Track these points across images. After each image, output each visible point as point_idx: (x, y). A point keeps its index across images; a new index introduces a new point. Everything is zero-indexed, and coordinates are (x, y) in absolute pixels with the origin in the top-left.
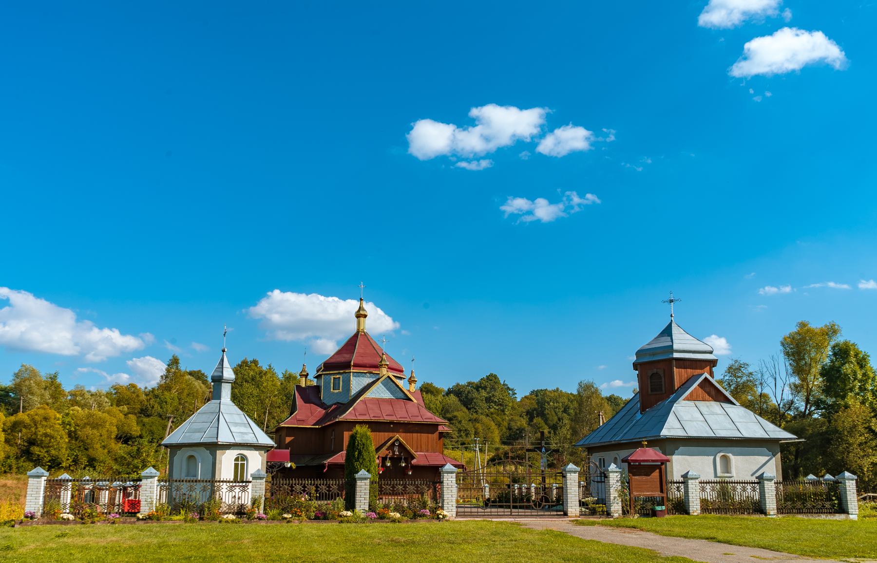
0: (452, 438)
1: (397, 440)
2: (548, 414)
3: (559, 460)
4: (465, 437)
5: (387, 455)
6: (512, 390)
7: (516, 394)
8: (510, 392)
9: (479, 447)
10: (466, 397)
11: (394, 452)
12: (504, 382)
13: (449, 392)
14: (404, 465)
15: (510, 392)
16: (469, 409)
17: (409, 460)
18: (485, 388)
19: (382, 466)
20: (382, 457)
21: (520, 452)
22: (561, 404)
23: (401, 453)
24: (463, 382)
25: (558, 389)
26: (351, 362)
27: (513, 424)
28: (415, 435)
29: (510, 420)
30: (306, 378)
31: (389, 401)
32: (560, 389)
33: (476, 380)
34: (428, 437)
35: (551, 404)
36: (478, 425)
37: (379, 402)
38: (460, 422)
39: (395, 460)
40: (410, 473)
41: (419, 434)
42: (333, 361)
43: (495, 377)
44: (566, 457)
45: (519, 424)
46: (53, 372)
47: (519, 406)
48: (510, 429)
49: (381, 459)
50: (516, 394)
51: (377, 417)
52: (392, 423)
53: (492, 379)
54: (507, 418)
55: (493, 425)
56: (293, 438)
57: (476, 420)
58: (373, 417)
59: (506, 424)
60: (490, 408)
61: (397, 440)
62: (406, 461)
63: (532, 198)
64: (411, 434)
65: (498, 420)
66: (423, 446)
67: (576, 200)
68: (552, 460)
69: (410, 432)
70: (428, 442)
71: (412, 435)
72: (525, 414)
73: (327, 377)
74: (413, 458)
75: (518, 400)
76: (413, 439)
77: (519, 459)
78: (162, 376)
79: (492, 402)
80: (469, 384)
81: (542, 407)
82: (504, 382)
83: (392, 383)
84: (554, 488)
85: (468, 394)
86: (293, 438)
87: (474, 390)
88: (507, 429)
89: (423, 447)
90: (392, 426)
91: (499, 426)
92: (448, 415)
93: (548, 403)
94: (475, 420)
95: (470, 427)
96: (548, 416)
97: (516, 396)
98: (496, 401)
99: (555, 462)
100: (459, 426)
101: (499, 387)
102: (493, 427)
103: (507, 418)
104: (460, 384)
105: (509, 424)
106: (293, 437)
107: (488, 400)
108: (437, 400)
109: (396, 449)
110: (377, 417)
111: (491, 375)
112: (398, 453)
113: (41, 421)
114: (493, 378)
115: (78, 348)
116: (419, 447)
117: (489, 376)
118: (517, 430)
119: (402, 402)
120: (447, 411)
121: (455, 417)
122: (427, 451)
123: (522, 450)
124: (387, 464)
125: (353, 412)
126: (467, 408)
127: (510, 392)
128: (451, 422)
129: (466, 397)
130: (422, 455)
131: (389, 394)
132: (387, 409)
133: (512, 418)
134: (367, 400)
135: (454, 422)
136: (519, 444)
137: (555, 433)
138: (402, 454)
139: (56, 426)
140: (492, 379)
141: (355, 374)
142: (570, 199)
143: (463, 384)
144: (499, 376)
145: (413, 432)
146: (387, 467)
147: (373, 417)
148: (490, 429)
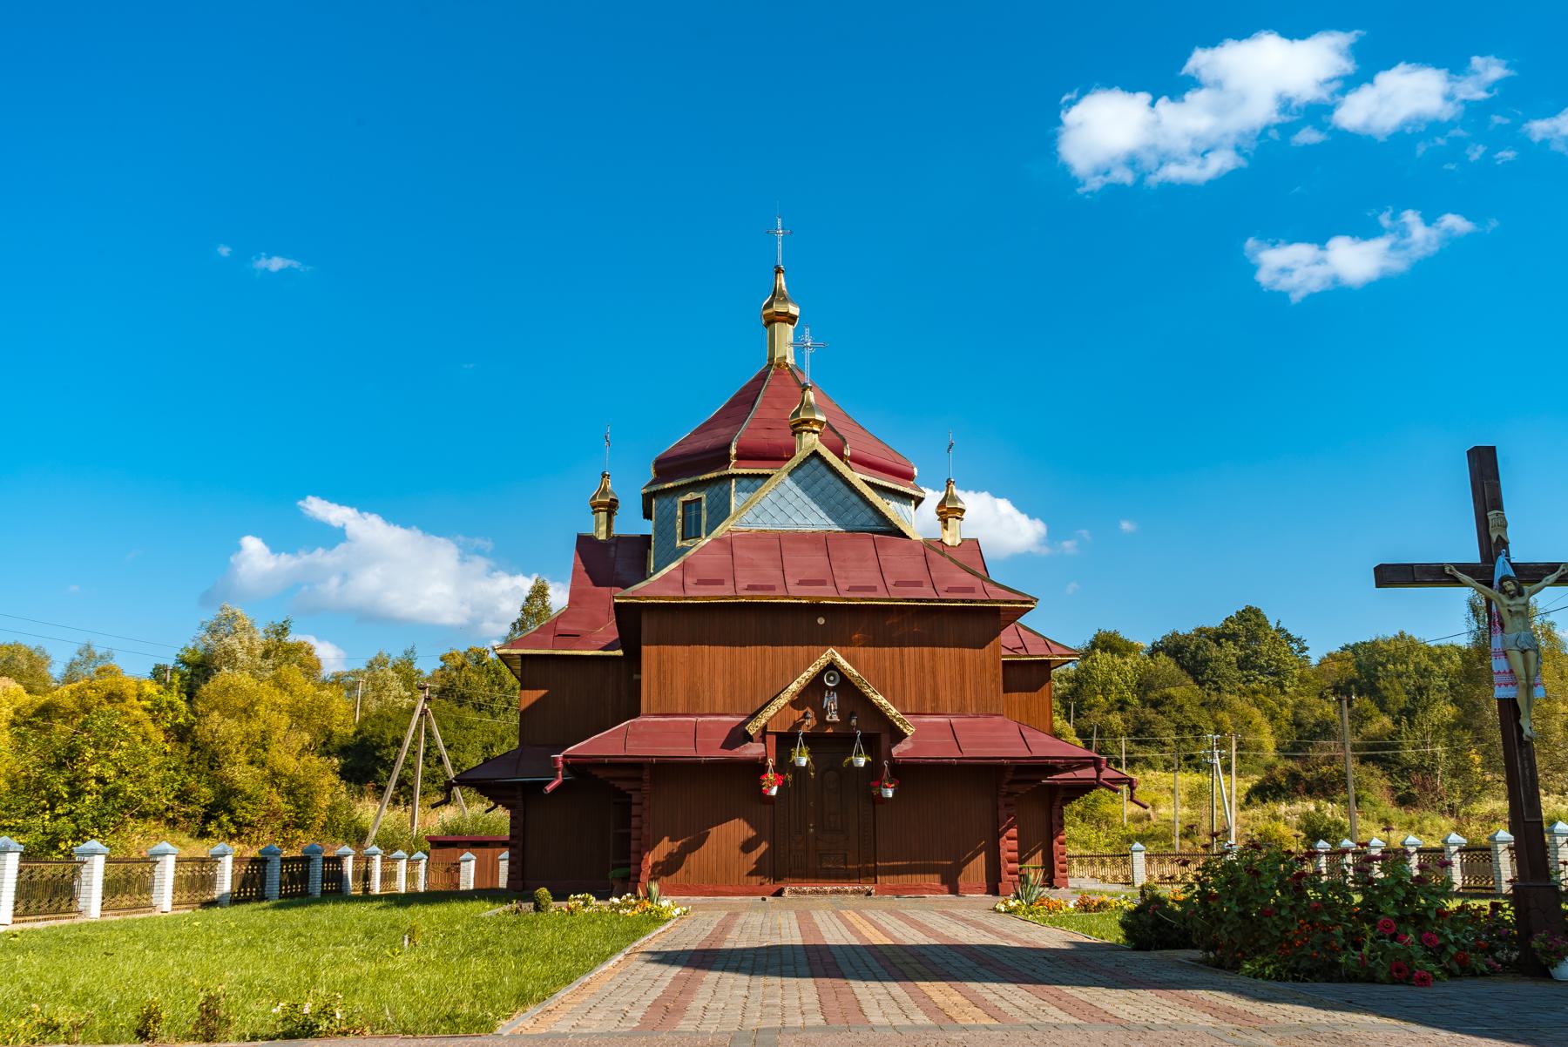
0: (1164, 744)
1: (832, 666)
2: (1386, 688)
3: (1424, 787)
4: (1193, 743)
5: (798, 725)
6: (1298, 641)
7: (1307, 649)
8: (1295, 646)
9: (1220, 755)
10: (1194, 657)
11: (821, 713)
12: (1278, 624)
13: (1155, 650)
14: (862, 761)
15: (1295, 646)
16: (1201, 684)
17: (884, 745)
18: (1233, 637)
19: (777, 769)
20: (777, 734)
21: (1324, 769)
22: (1411, 667)
23: (852, 714)
24: (1186, 629)
25: (1402, 635)
26: (729, 445)
27: (1304, 713)
28: (910, 652)
29: (1296, 706)
30: (610, 515)
31: (822, 541)
32: (1408, 633)
33: (1215, 622)
34: (962, 660)
35: (1390, 666)
36: (1223, 716)
37: (780, 544)
38: (1180, 709)
39: (826, 743)
40: (890, 793)
41: (926, 649)
42: (680, 451)
43: (1257, 613)
44: (1442, 780)
45: (1318, 712)
46: (279, 620)
47: (1315, 674)
48: (1297, 724)
49: (772, 740)
50: (1307, 649)
51: (762, 588)
52: (816, 608)
53: (1250, 618)
54: (1290, 702)
55: (1258, 716)
56: (543, 692)
57: (1220, 705)
58: (750, 588)
59: (1287, 712)
60: (1248, 680)
61: (832, 666)
62: (871, 745)
63: (1320, 238)
64: (897, 649)
65: (1270, 705)
66: (942, 694)
67: (1419, 232)
68: (1408, 788)
69: (890, 643)
70: (962, 677)
71: (902, 654)
72: (1331, 690)
73: (666, 502)
74: (899, 736)
75: (1314, 661)
76: (902, 664)
77: (1324, 788)
78: (514, 624)
79: (1254, 668)
80: (1200, 631)
81: (1368, 676)
82: (1278, 624)
83: (830, 477)
84: (1453, 849)
85: (1196, 653)
86: (543, 692)
87: (1210, 643)
88: (1292, 725)
89: (945, 695)
90: (821, 621)
91: (1272, 718)
92: (1152, 695)
93: (1383, 665)
94: (1215, 703)
95: (1203, 719)
96: (1385, 693)
97: (1307, 653)
98: (1262, 666)
99: (1415, 791)
100: (1179, 717)
101: (1266, 634)
102: (1258, 720)
103: (1290, 702)
104: (1180, 633)
105: (1295, 714)
106: (545, 689)
107: (1243, 664)
108: (1125, 663)
109: (831, 703)
110: (762, 588)
111: (1249, 609)
112: (836, 718)
113: (100, 703)
114: (1253, 616)
115: (466, 609)
116: (928, 696)
117: (1243, 611)
118: (1315, 725)
119: (866, 543)
120: (1150, 687)
121: (1168, 697)
122: (961, 712)
123: (1330, 765)
124: (795, 757)
125: (679, 575)
126: (1196, 681)
127: (1292, 645)
128: (1161, 709)
129: (1194, 657)
130: (937, 726)
131: (823, 515)
132: (815, 563)
133: (1301, 702)
134: (739, 537)
135: (1167, 708)
136: (1322, 749)
137: (1411, 723)
138: (854, 722)
139: (136, 712)
140: (1250, 618)
141: (745, 482)
142: (1404, 232)
143: (1187, 632)
144: (1264, 611)
145: (901, 644)
146: (800, 772)
147: (750, 588)
148: (1250, 722)
